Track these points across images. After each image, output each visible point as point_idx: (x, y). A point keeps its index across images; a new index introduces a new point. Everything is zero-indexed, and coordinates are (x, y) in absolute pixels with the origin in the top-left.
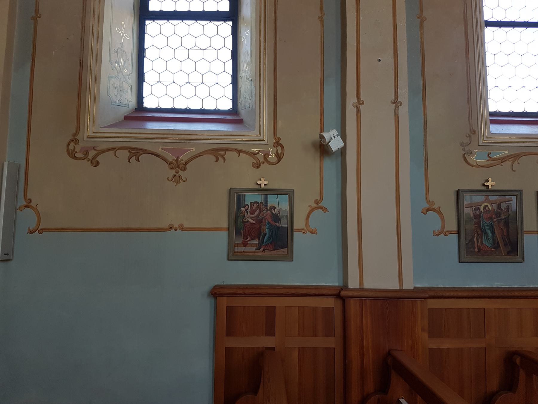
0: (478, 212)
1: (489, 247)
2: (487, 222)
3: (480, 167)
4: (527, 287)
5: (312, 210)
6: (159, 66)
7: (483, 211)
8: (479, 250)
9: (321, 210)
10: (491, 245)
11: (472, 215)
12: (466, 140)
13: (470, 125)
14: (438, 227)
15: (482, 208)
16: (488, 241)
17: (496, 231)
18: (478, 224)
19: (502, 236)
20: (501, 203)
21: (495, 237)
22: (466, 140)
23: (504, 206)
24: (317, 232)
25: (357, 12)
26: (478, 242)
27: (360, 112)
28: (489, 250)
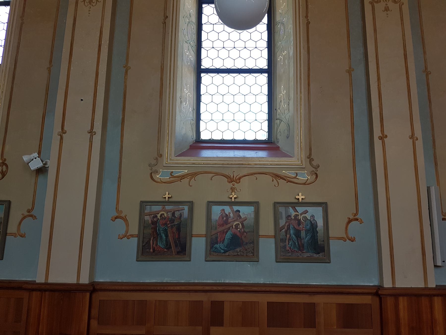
0: (155, 219)
1: (163, 248)
2: (162, 227)
3: (163, 183)
4: (193, 282)
5: (24, 217)
6: (212, 108)
7: (159, 218)
8: (154, 250)
9: (31, 218)
10: (164, 247)
11: (150, 222)
12: (154, 162)
13: (158, 150)
14: (123, 232)
15: (159, 216)
16: (162, 243)
17: (169, 235)
18: (155, 229)
19: (174, 238)
20: (175, 212)
21: (168, 240)
22: (154, 162)
23: (177, 214)
24: (26, 236)
25: (69, 64)
26: (153, 243)
27: (63, 138)
28: (162, 250)
